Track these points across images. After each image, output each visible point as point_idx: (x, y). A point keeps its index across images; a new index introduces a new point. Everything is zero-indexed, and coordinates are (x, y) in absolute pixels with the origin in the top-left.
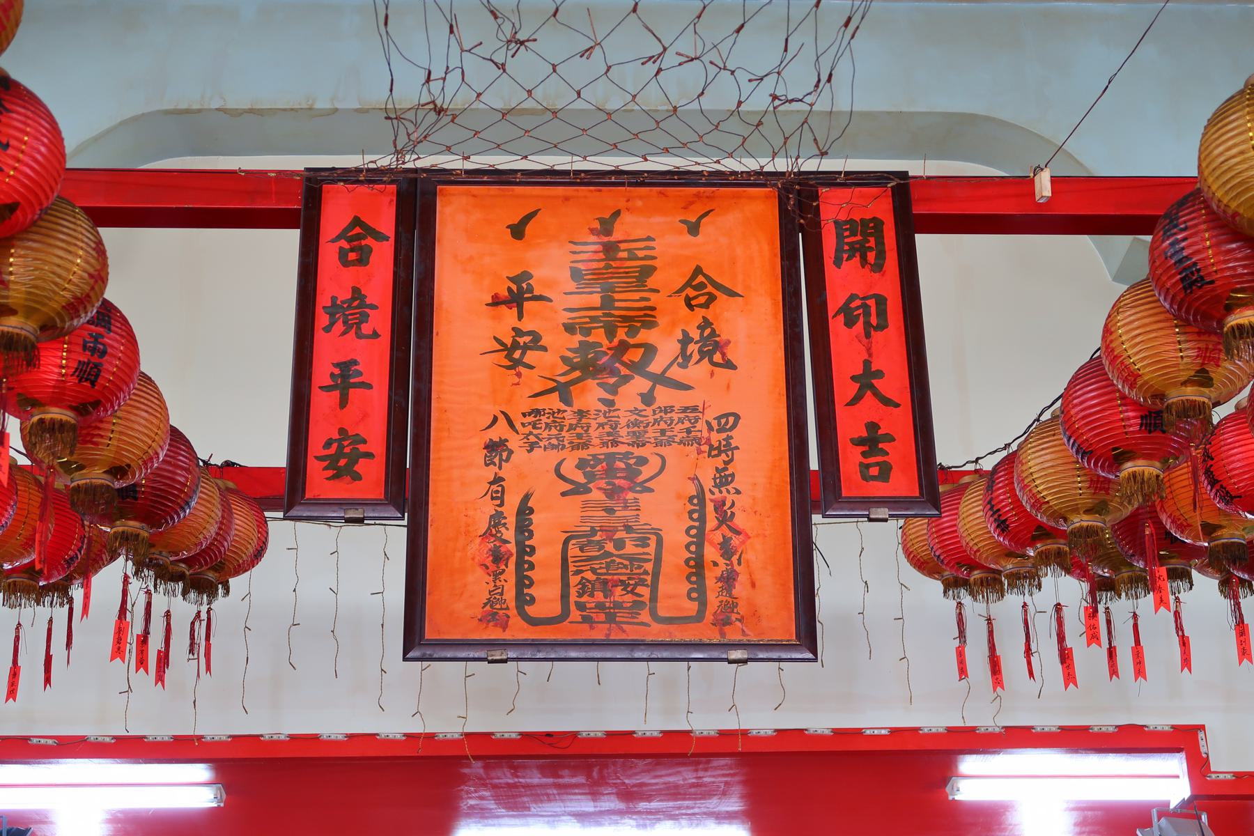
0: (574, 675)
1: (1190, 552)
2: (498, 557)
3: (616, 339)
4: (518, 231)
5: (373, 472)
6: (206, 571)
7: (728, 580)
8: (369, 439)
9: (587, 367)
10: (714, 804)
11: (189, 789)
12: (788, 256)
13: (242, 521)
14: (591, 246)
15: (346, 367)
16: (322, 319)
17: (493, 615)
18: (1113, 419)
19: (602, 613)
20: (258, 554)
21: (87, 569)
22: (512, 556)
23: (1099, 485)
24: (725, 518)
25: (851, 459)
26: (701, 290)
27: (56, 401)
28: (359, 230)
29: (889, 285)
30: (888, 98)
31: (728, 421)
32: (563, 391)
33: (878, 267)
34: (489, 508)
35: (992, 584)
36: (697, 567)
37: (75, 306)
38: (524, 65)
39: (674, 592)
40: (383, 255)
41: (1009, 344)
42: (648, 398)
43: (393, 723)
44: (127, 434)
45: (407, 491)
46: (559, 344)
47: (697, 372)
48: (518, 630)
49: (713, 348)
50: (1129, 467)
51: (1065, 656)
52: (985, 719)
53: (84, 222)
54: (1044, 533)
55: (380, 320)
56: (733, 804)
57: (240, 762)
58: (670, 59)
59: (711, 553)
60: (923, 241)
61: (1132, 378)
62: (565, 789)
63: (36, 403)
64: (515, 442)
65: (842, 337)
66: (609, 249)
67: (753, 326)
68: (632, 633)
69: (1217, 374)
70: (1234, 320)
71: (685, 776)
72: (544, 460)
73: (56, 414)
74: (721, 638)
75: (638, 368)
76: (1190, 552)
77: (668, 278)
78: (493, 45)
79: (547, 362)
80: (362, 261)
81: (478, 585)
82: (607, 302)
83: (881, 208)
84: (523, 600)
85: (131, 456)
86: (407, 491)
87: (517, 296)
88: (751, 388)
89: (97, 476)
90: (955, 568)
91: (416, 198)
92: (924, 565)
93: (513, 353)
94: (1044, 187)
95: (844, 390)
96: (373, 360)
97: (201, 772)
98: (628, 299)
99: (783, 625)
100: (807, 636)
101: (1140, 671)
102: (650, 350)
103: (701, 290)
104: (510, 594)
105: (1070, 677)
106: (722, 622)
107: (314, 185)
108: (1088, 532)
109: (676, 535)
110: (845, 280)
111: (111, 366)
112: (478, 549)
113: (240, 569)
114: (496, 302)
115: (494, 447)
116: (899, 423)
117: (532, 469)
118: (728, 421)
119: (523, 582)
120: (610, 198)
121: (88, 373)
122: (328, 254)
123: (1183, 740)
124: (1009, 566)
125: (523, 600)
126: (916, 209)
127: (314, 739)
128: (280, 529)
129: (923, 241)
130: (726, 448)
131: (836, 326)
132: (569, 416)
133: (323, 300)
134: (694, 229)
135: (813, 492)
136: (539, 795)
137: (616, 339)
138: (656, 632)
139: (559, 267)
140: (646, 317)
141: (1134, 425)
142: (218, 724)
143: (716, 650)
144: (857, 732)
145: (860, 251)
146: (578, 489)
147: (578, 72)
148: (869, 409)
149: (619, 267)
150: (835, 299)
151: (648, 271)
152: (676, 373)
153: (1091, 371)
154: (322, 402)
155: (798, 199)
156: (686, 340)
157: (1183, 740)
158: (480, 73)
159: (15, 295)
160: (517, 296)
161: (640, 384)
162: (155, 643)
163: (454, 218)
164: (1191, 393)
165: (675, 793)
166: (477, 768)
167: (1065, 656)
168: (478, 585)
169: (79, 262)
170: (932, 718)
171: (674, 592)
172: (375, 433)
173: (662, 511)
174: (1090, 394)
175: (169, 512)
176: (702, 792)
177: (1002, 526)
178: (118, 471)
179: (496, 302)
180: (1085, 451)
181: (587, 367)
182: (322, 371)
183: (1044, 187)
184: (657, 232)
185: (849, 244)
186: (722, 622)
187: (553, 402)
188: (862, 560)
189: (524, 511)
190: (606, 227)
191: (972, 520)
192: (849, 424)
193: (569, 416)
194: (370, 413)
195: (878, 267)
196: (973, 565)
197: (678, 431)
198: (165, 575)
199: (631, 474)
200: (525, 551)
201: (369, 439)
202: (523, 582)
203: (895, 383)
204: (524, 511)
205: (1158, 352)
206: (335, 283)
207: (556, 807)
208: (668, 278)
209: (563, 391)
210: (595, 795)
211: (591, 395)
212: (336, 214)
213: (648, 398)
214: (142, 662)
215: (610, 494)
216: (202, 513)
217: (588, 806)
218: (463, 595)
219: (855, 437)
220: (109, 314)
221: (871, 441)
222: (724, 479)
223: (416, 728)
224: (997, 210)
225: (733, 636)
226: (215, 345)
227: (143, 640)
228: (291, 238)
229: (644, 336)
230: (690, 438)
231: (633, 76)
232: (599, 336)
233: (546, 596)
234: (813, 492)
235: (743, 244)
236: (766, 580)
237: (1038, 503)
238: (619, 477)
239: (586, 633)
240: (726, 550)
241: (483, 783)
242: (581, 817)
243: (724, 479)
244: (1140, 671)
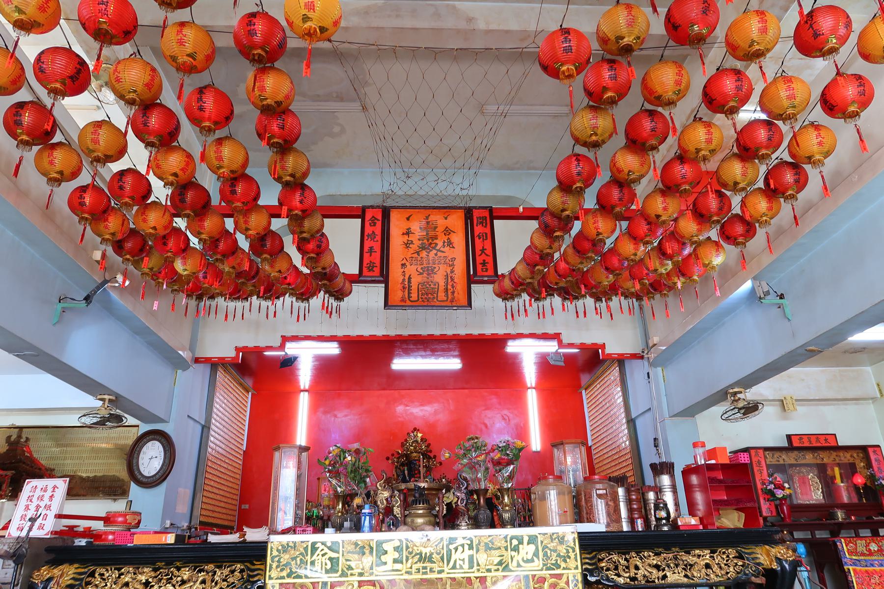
0: (421, 314)
1: (553, 289)
2: (404, 288)
3: (429, 243)
4: (408, 219)
5: (377, 270)
6: (340, 295)
7: (453, 293)
8: (376, 267)
9: (423, 248)
10: (452, 353)
11: (332, 349)
12: (466, 224)
13: (347, 284)
14: (424, 222)
15: (371, 248)
16: (366, 238)
17: (403, 300)
18: (535, 258)
19: (426, 299)
20: (350, 292)
21: (314, 294)
22: (407, 287)
23: (532, 272)
24: (452, 280)
25: (479, 267)
26: (448, 231)
27: (312, 252)
28: (374, 219)
29: (488, 231)
30: (486, 188)
31: (453, 259)
32: (418, 253)
33: (486, 227)
34: (402, 278)
35: (512, 297)
36: (446, 290)
37: (318, 232)
38: (410, 182)
39: (441, 295)
40: (379, 224)
41: (513, 242)
42: (436, 255)
43: (380, 332)
44: (325, 261)
45: (384, 278)
46: (417, 243)
47: (446, 249)
48: (408, 303)
49: (450, 244)
50: (537, 268)
51: (526, 311)
52: (513, 332)
53: (320, 217)
54: (522, 284)
55: (378, 238)
56: (456, 353)
57: (346, 342)
58: (440, 181)
59: (449, 287)
60: (495, 221)
61: (536, 248)
62: (418, 349)
63: (308, 253)
64: (407, 264)
65: (478, 242)
66: (428, 223)
67: (459, 239)
68: (433, 304)
69: (553, 247)
70: (555, 234)
71: (445, 346)
72: (414, 267)
73: (312, 255)
74: (451, 304)
75: (434, 248)
76: (553, 289)
77: (440, 229)
78: (403, 178)
79: (414, 247)
80: (374, 225)
81: (400, 294)
82: (427, 234)
83: (486, 214)
84: (409, 297)
85: (326, 265)
86: (384, 278)
87: (408, 233)
88: (458, 253)
89: (319, 270)
90: (505, 295)
91: (386, 212)
92: (498, 295)
93: (407, 245)
94: (521, 210)
95: (478, 252)
96: (377, 247)
97: (335, 345)
98: (432, 233)
99: (464, 302)
100: (470, 305)
101: (544, 317)
102: (436, 244)
103: (448, 231)
104: (407, 296)
105: (527, 315)
106: (452, 301)
107: (364, 209)
108: (530, 283)
109: (442, 283)
110: (478, 229)
111: (324, 245)
112: (400, 286)
113: (347, 295)
114: (403, 234)
115: (403, 265)
116: (490, 260)
117: (411, 269)
118: (453, 259)
119: (409, 293)
120: (428, 212)
121: (319, 246)
122: (367, 224)
123: (556, 337)
124: (515, 293)
125: (409, 297)
126: (494, 214)
127: (362, 336)
128: (355, 287)
129: (495, 221)
130: (453, 265)
131: (477, 239)
132: (419, 258)
133: (366, 234)
134: (446, 219)
135: (471, 280)
136: (412, 351)
137: (429, 243)
138: (438, 303)
139: (417, 227)
140: (436, 237)
141: (538, 258)
142: (340, 333)
143: (450, 307)
144: (484, 335)
145: (482, 223)
146: (421, 274)
147: (421, 183)
148: (484, 257)
149: (430, 226)
150: (476, 234)
151: (436, 227)
152: (442, 249)
153: (529, 247)
154: (366, 255)
155: (468, 213)
156: (444, 242)
157: (556, 337)
158: (401, 184)
159: (306, 229)
160: (408, 233)
161: (434, 252)
162: (330, 309)
163: (394, 216)
164: (548, 251)
165: (443, 350)
166: (398, 344)
167: (526, 311)
168: (400, 294)
169: (318, 223)
170: (501, 331)
171: (441, 295)
172: (377, 262)
173: (439, 278)
174: (529, 252)
175: (333, 280)
176: (449, 350)
177: (513, 283)
178: (324, 269)
179: (403, 234)
180: (528, 264)
181: (423, 248)
182: (366, 249)
183: (521, 210)
184: (439, 220)
185: (479, 220)
186: (452, 301)
187: (416, 255)
188: (483, 294)
189: (410, 278)
190: (427, 218)
191: (507, 283)
192: (479, 260)
193: (419, 258)
194: (376, 258)
195: (486, 227)
196: (508, 294)
197: (442, 261)
198: (331, 295)
199: (433, 270)
200: (410, 287)
201: (376, 267)
202: (409, 293)
203: (489, 251)
204: (410, 278)
205: (542, 242)
206: (368, 230)
207: (416, 354)
208: (440, 229)
209: (418, 253)
210: (425, 351)
211: (424, 254)
212: (369, 215)
213: (436, 255)
214: (327, 312)
215: (428, 274)
216: (340, 280)
217: (423, 353)
218: (397, 295)
219: (481, 267)
220: (323, 235)
221: (484, 263)
222: (452, 272)
223: (385, 334)
224: (511, 215)
225: (454, 304)
226: (344, 242)
227: (327, 308)
228: (358, 221)
229: (435, 241)
230: (445, 263)
231: (433, 184)
232: (425, 241)
233: (414, 296)
234: (471, 280)
235: (456, 221)
236: (461, 292)
237: (520, 277)
238: (430, 271)
239: (422, 304)
240: (453, 286)
241: (400, 348)
242: (422, 356)
243: (452, 272)
244: (544, 317)
